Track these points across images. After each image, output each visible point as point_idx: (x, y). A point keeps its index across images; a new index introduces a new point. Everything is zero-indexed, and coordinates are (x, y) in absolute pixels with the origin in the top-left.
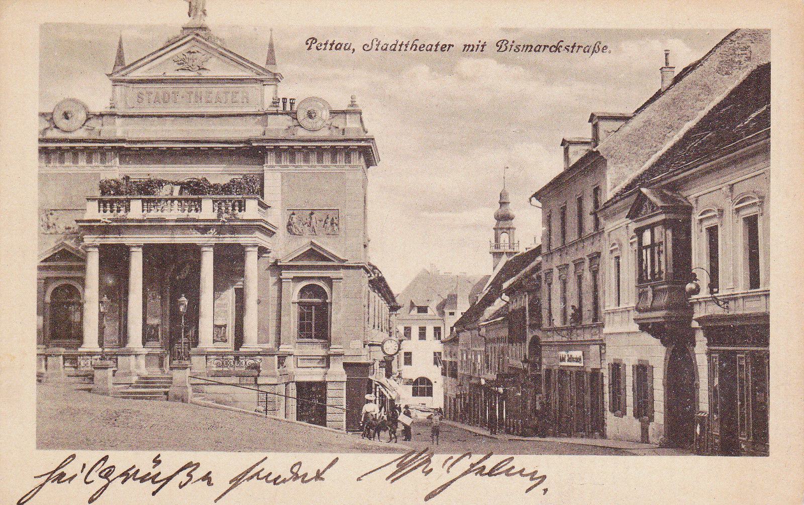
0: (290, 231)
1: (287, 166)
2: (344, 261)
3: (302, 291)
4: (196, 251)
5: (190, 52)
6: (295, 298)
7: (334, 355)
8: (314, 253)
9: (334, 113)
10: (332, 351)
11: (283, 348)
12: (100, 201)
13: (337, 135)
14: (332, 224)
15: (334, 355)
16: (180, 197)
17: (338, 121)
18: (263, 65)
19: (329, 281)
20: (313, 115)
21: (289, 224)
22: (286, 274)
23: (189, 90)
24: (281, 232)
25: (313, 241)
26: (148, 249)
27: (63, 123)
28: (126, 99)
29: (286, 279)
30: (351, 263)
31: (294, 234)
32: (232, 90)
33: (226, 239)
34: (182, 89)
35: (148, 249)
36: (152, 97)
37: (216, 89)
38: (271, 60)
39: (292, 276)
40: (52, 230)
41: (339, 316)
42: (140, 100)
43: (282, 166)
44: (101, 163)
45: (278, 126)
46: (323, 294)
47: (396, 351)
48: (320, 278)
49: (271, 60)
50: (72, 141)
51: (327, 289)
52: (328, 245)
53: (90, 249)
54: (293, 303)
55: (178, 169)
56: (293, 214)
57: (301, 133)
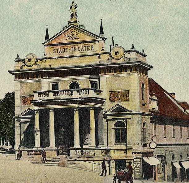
0: (110, 100)
1: (124, 74)
2: (131, 111)
3: (116, 125)
4: (71, 111)
5: (71, 32)
6: (113, 127)
7: (129, 149)
8: (120, 109)
9: (125, 52)
10: (128, 148)
11: (109, 147)
12: (53, 92)
13: (127, 61)
14: (126, 97)
15: (129, 149)
16: (53, 91)
17: (127, 55)
18: (98, 35)
19: (126, 120)
20: (117, 53)
21: (110, 97)
22: (109, 118)
23: (72, 47)
24: (107, 101)
25: (30, 108)
26: (55, 110)
27: (28, 63)
28: (49, 52)
29: (109, 119)
30: (134, 112)
31: (112, 101)
32: (87, 45)
33: (82, 105)
34: (69, 47)
35: (55, 110)
36: (59, 50)
37: (81, 46)
38: (102, 32)
39: (24, 121)
40: (26, 104)
41: (130, 134)
42: (55, 52)
43: (39, 79)
44: (120, 72)
45: (104, 59)
46: (124, 125)
47: (155, 147)
48: (123, 119)
49: (102, 32)
50: (119, 64)
51: (125, 123)
52: (123, 104)
53: (50, 111)
54: (112, 129)
55: (61, 78)
56: (111, 93)
57: (113, 61)
